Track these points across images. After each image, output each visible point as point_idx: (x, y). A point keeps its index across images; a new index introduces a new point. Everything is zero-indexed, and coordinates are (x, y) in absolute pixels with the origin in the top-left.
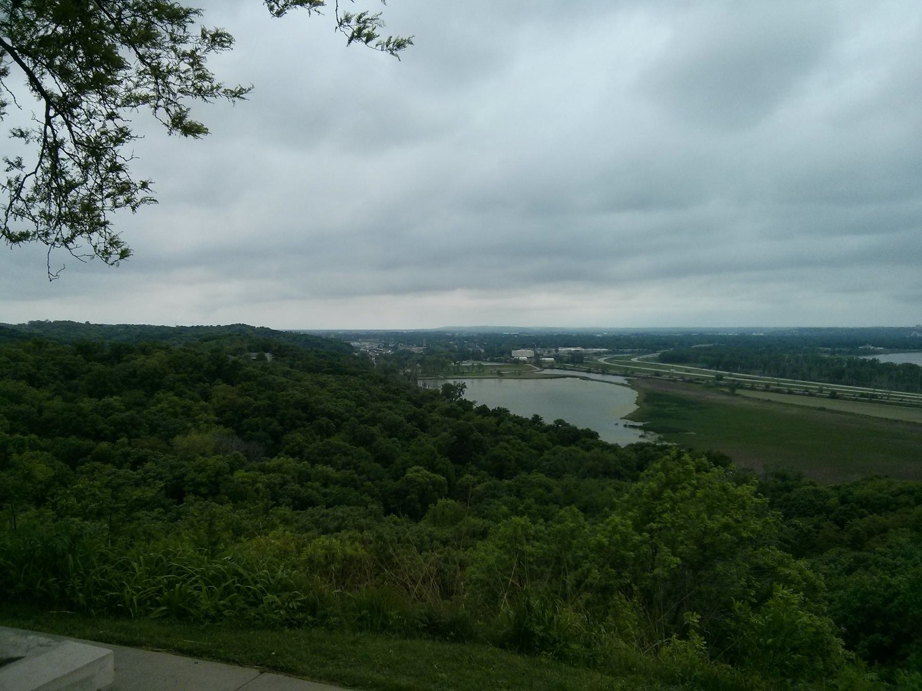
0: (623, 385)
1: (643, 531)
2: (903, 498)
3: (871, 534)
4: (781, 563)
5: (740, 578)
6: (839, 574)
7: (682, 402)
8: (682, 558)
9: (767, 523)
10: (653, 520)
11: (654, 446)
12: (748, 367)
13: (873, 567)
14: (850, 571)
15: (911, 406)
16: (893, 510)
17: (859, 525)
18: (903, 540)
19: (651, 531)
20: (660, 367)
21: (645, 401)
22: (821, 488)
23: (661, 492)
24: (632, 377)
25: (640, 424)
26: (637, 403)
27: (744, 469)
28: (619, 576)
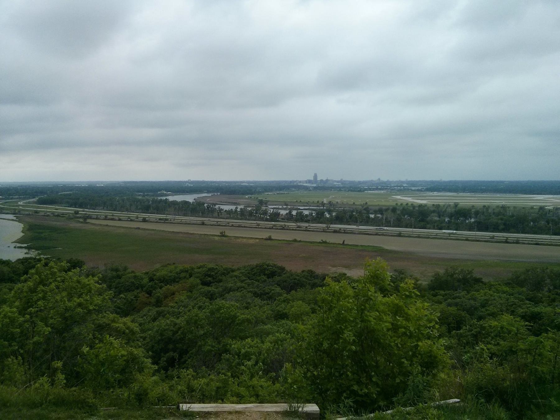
0: (13, 220)
1: (25, 314)
2: (183, 275)
3: (166, 297)
4: (113, 321)
5: (88, 334)
6: (149, 322)
7: (53, 229)
8: (52, 328)
9: (104, 299)
10: (32, 306)
11: (35, 259)
12: (94, 206)
13: (168, 315)
14: (154, 320)
15: (189, 224)
16: (178, 282)
17: (159, 293)
18: (182, 298)
19: (30, 314)
20: (38, 207)
21: (29, 230)
22: (137, 274)
23: (36, 288)
24: (19, 215)
25: (25, 245)
26: (23, 232)
27: (93, 268)
28: (10, 345)
